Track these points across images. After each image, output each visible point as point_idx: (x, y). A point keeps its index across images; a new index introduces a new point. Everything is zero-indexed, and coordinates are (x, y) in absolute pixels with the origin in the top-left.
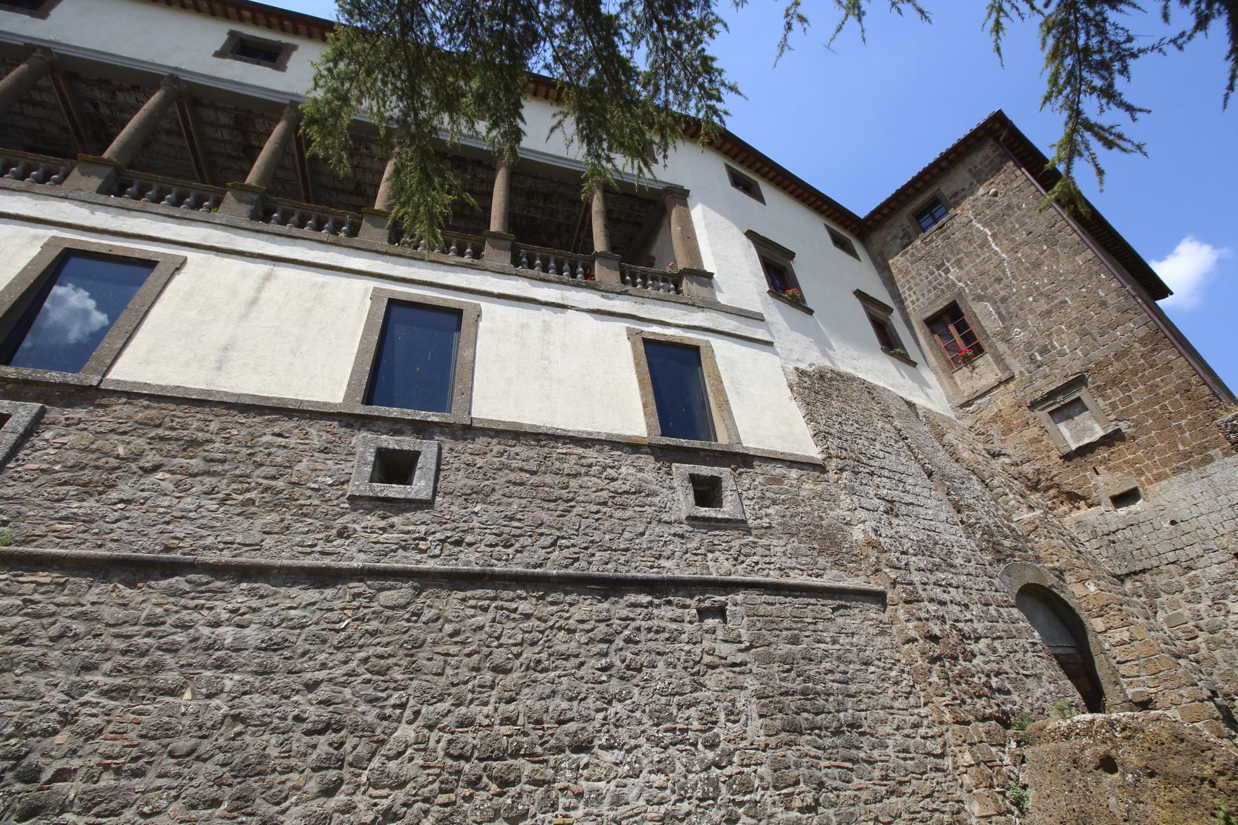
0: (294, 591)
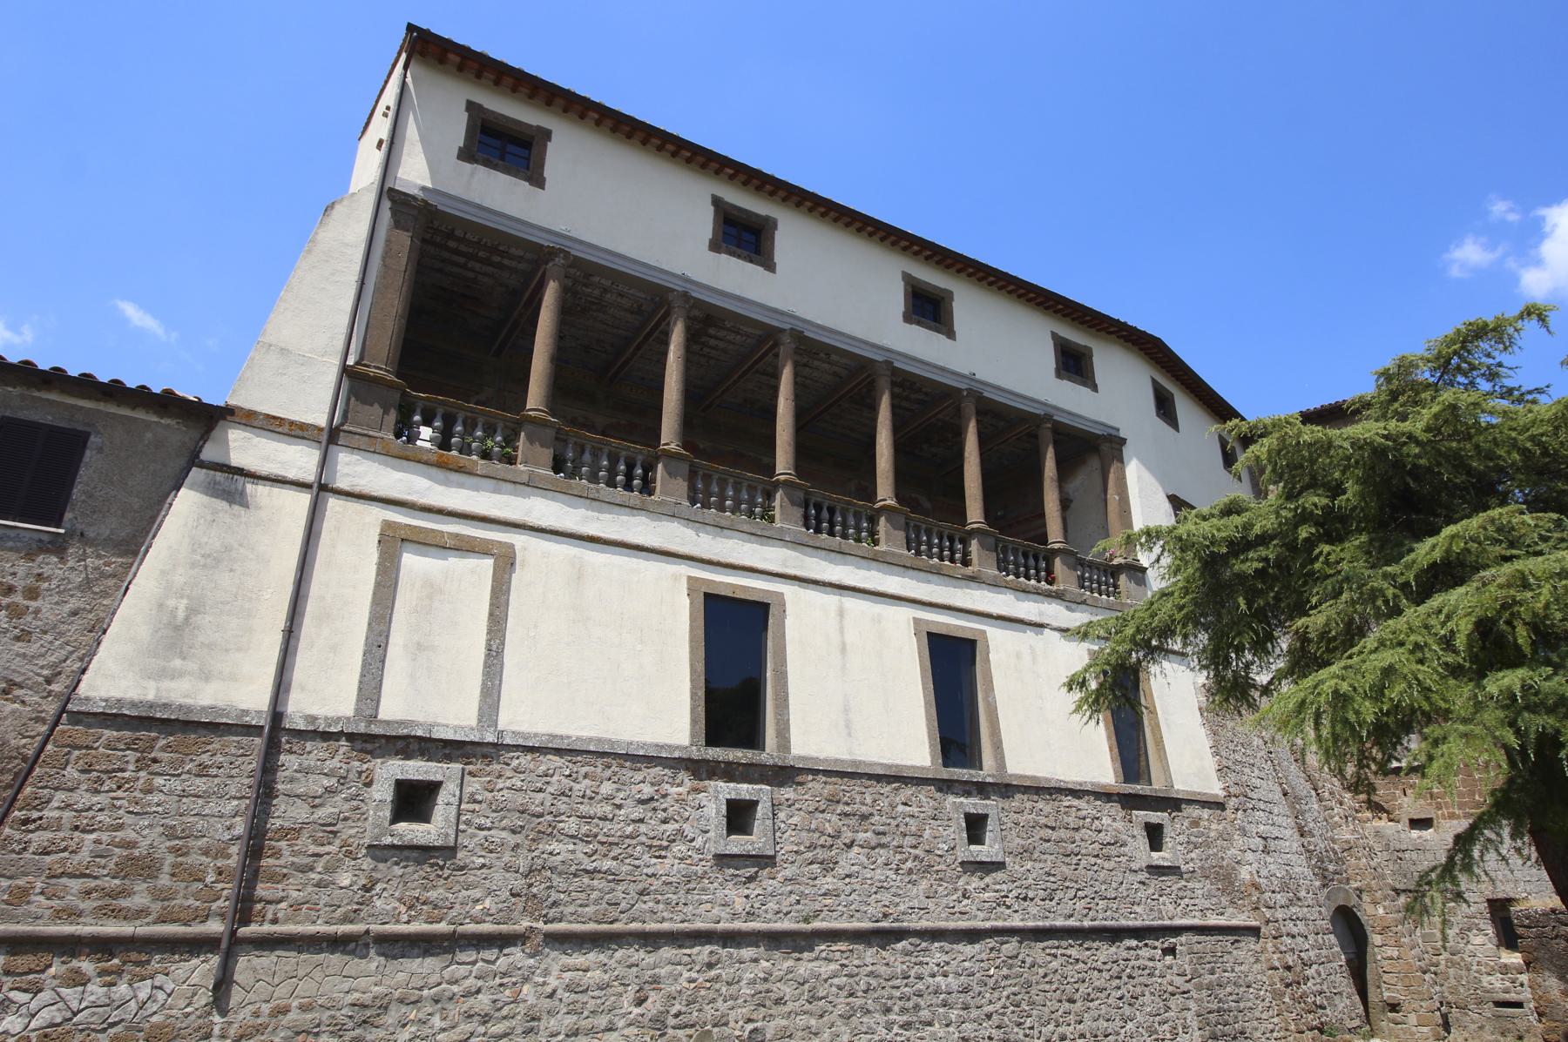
0: (960, 947)
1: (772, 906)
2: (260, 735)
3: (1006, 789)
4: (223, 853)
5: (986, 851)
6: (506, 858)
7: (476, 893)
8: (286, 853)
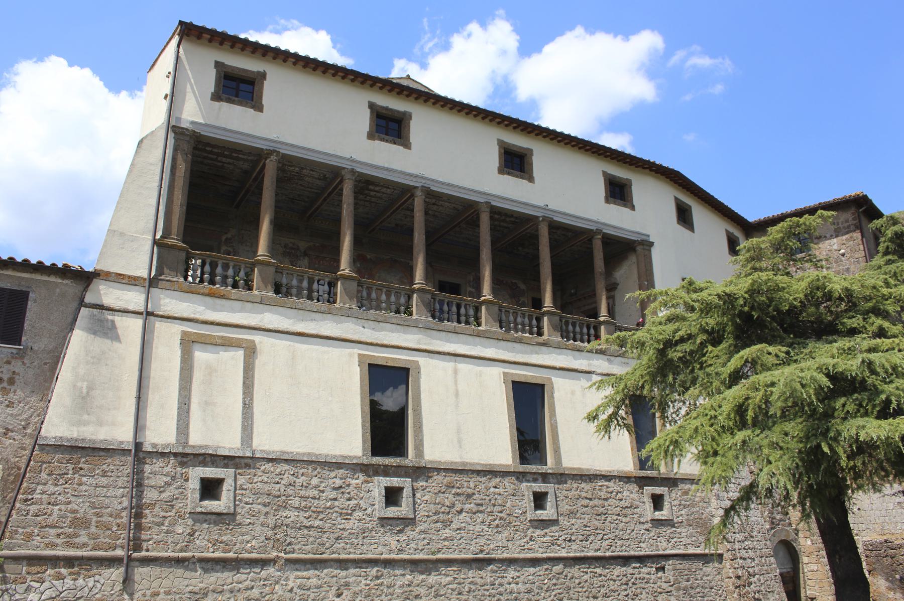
1: (413, 546)
2: (130, 455)
3: (561, 477)
4: (118, 516)
5: (548, 513)
6: (262, 519)
7: (248, 538)
8: (149, 516)
